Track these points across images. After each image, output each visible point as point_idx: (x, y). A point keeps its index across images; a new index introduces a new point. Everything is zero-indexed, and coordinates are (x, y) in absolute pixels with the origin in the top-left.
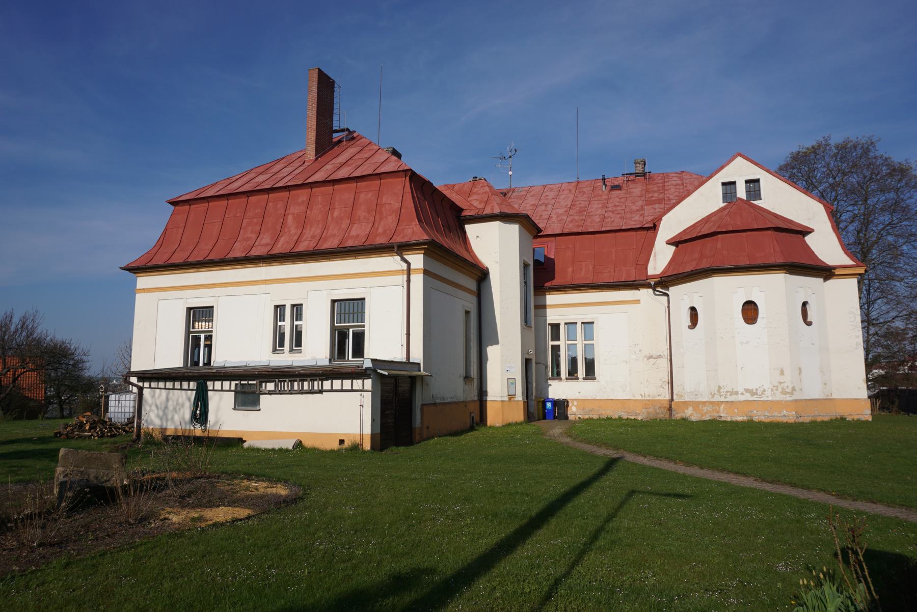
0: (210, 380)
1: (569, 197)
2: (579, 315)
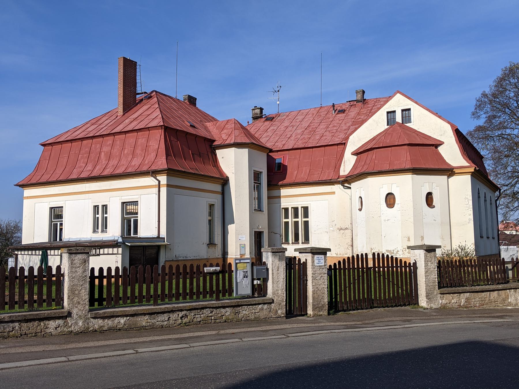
0: (49, 250)
1: (310, 120)
2: (299, 203)
